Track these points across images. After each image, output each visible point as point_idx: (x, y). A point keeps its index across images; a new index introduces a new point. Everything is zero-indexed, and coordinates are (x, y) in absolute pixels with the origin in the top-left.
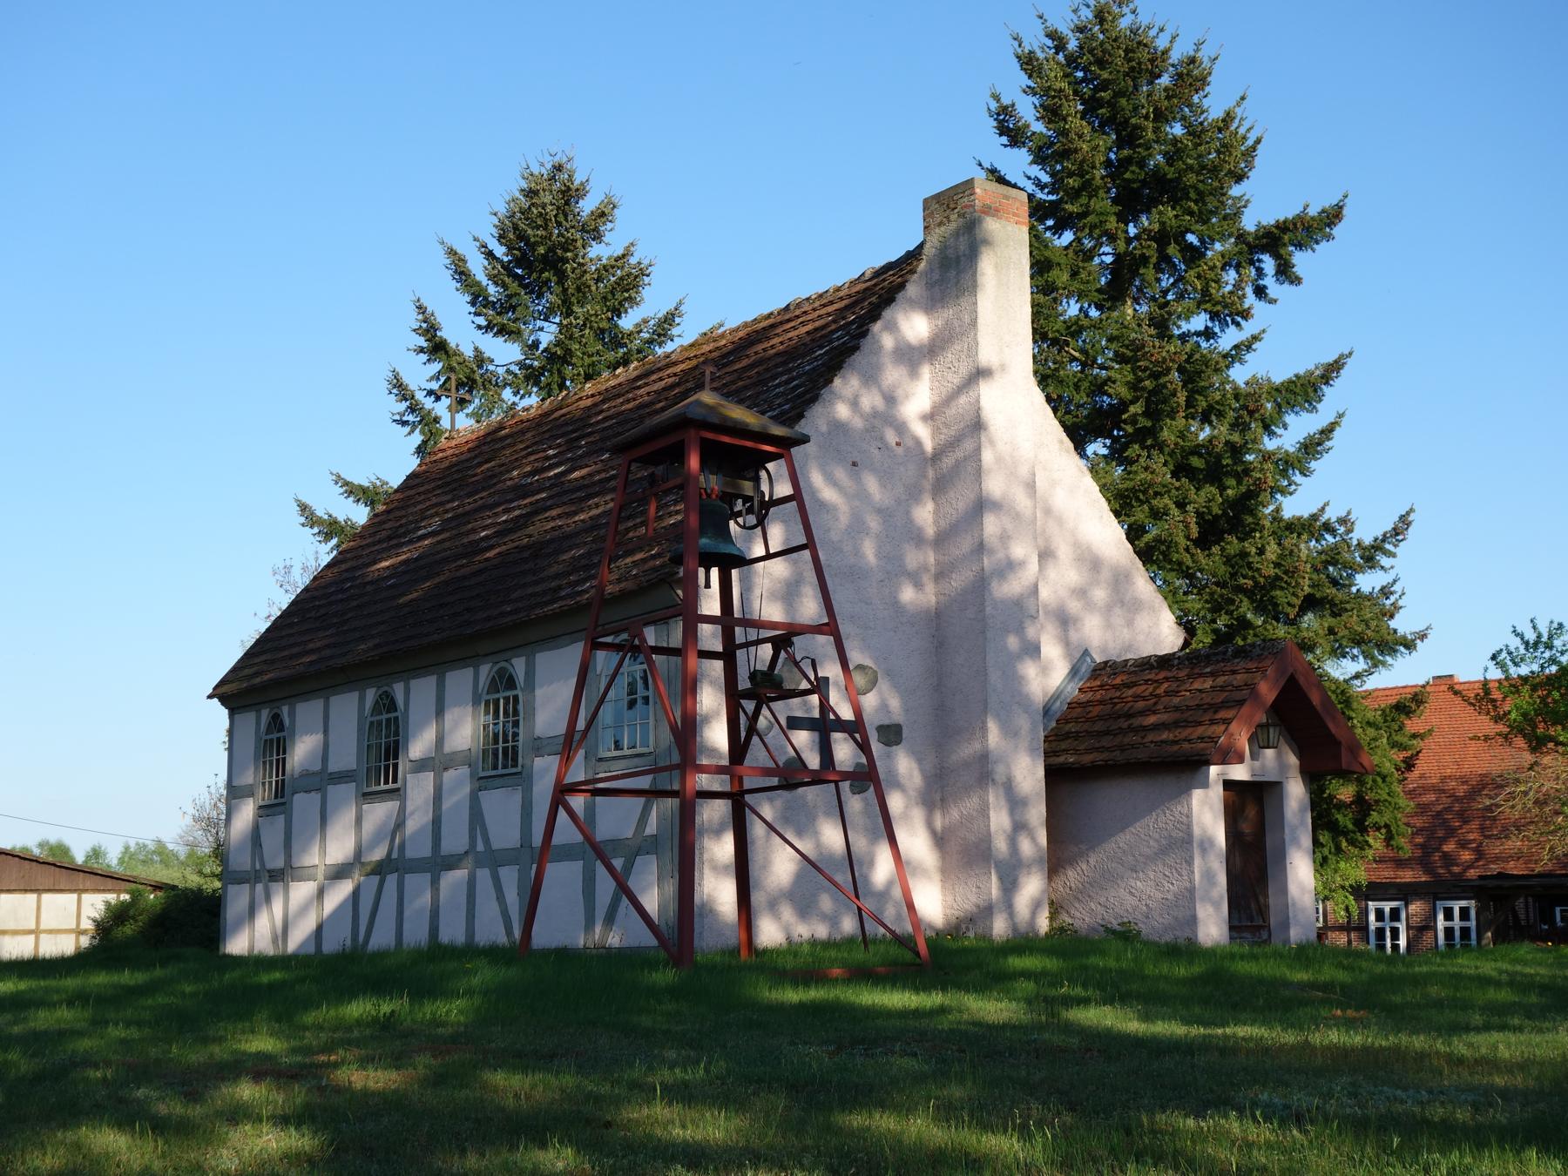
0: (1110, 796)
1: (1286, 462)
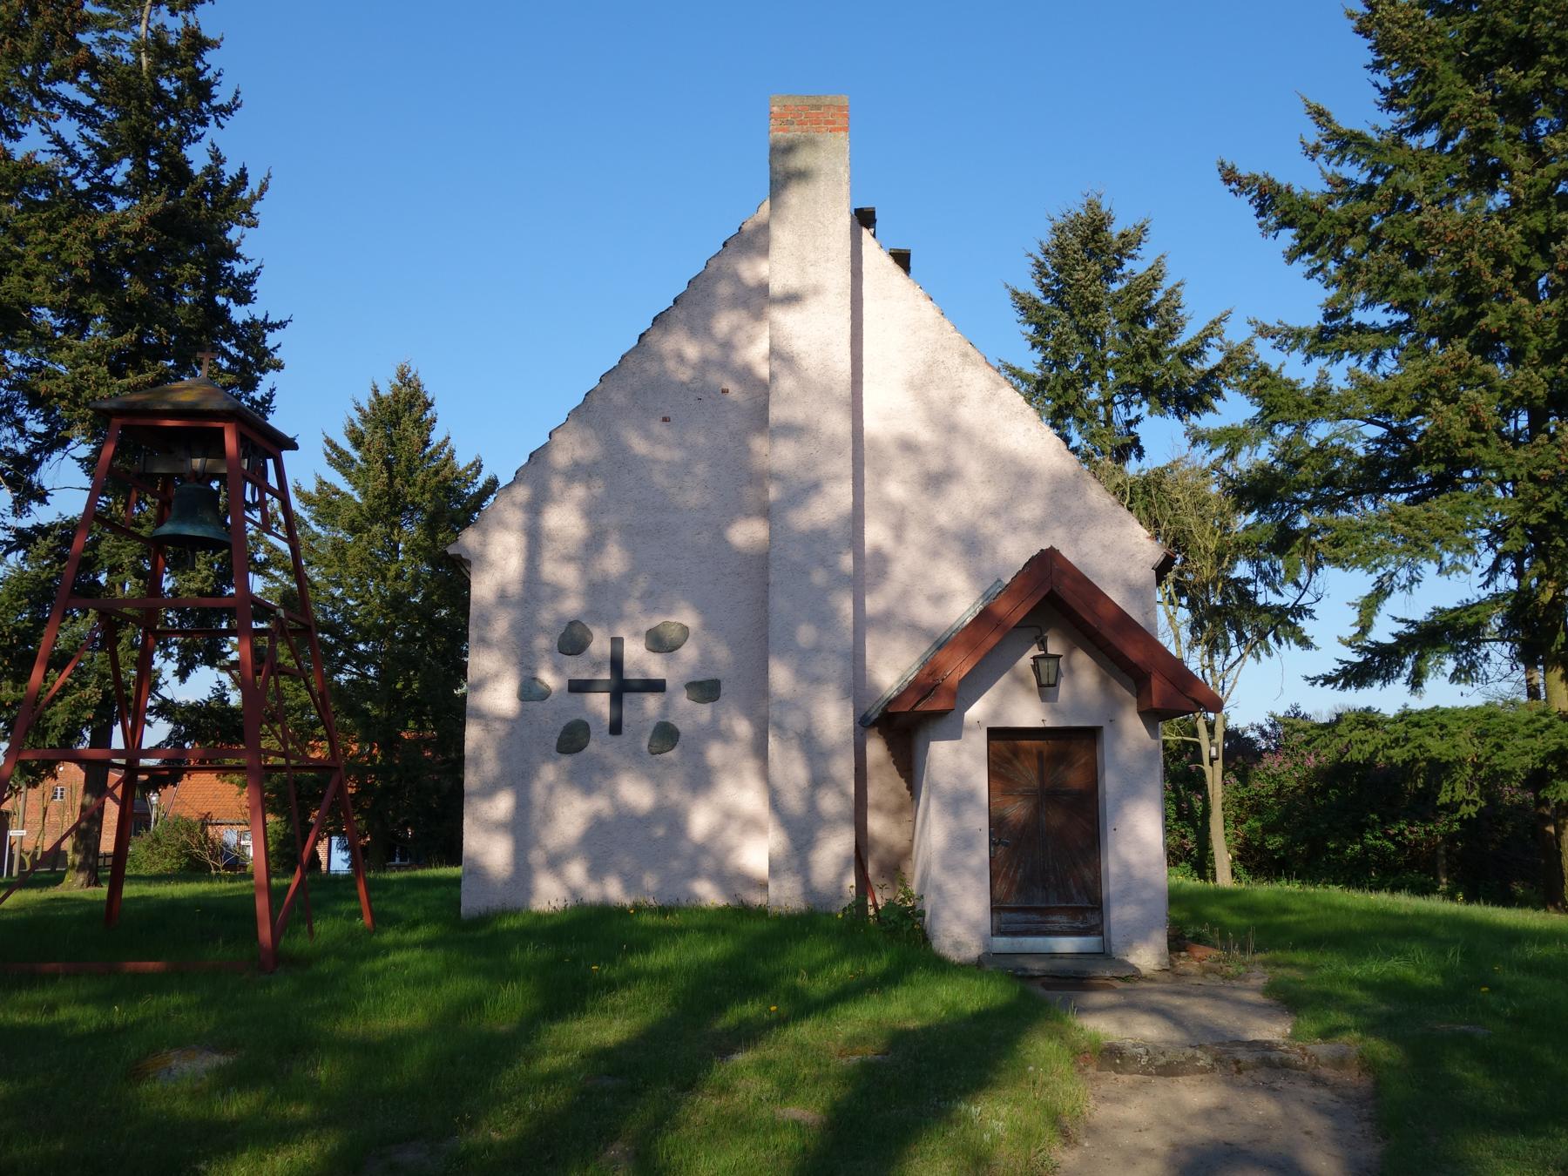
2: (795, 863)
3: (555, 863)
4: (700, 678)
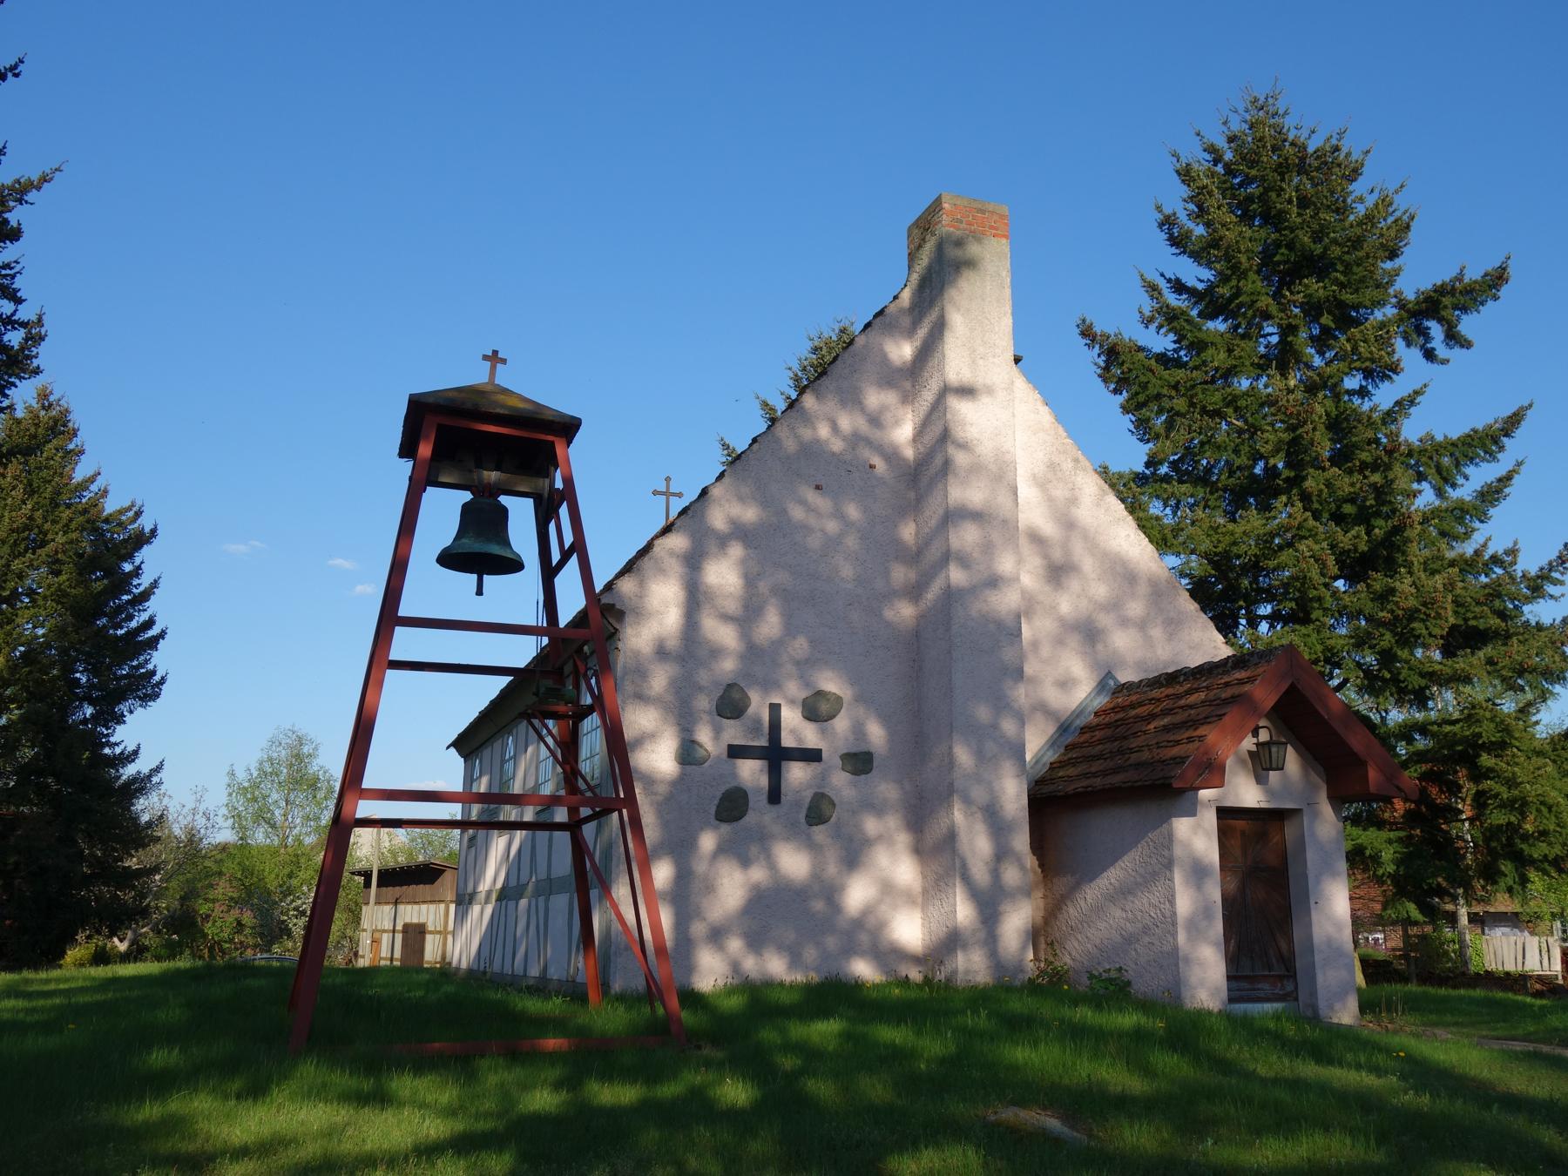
0: (1102, 825)
1: (1462, 510)
2: (982, 935)
3: (716, 936)
4: (854, 750)
